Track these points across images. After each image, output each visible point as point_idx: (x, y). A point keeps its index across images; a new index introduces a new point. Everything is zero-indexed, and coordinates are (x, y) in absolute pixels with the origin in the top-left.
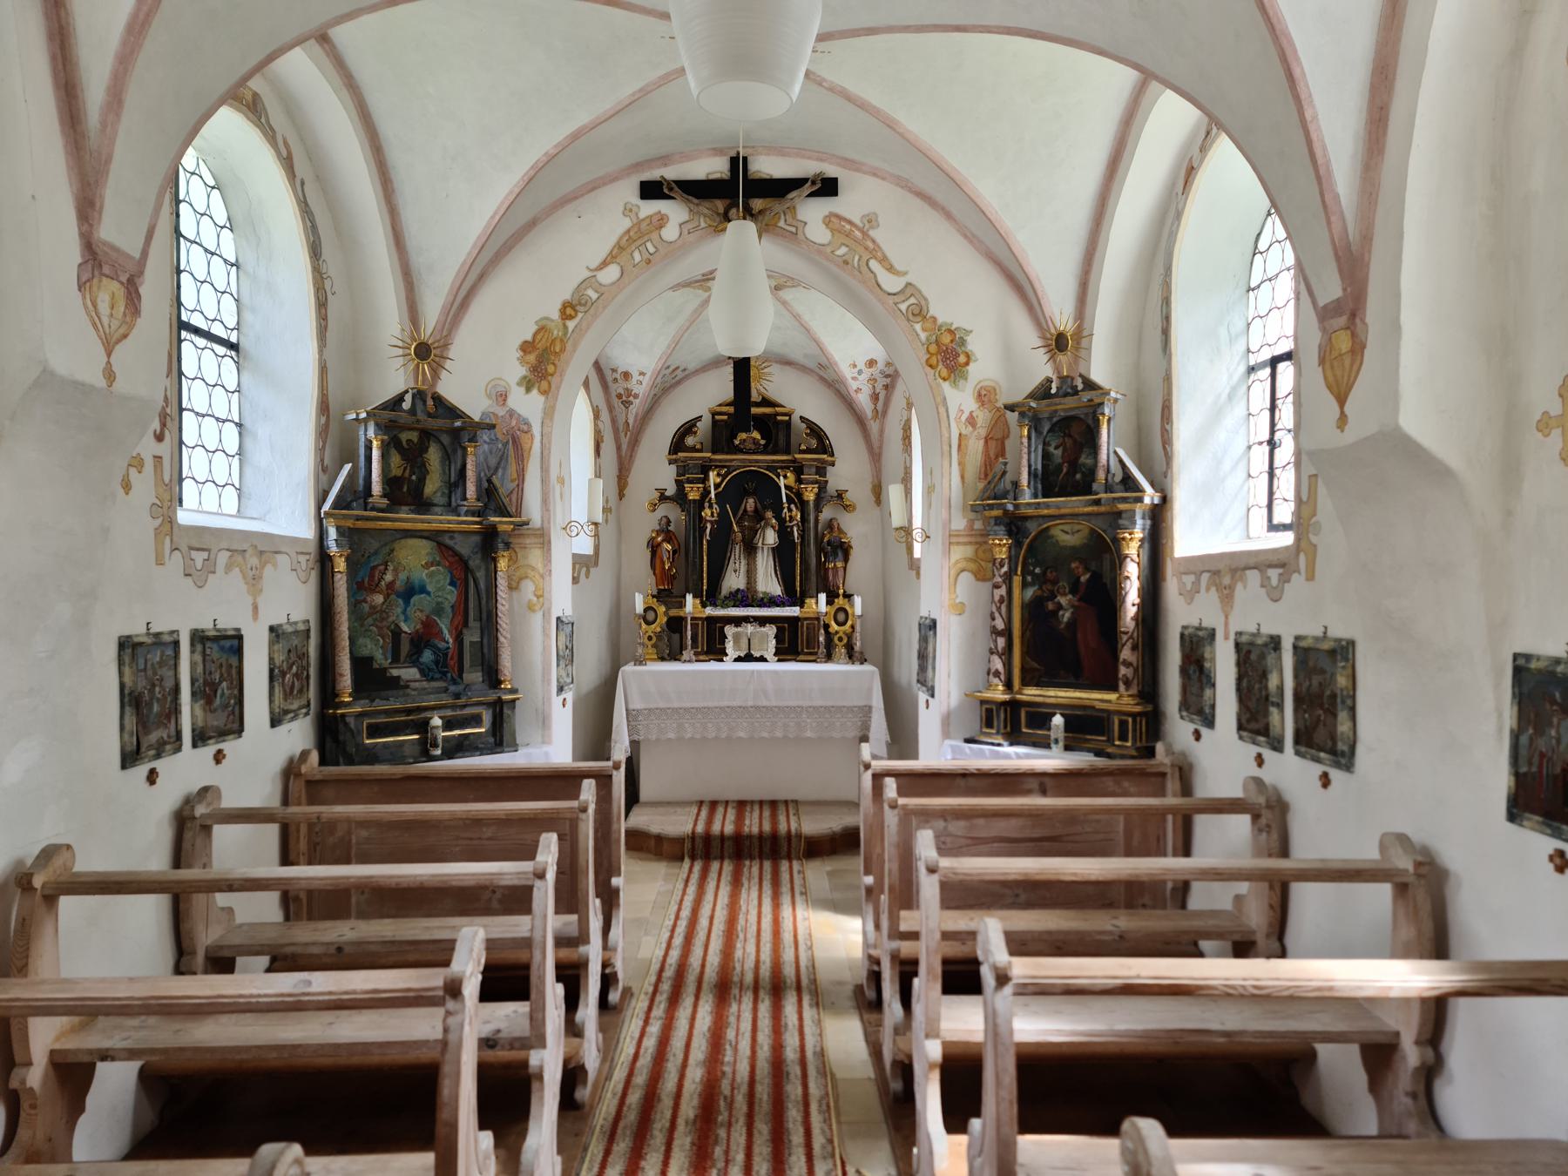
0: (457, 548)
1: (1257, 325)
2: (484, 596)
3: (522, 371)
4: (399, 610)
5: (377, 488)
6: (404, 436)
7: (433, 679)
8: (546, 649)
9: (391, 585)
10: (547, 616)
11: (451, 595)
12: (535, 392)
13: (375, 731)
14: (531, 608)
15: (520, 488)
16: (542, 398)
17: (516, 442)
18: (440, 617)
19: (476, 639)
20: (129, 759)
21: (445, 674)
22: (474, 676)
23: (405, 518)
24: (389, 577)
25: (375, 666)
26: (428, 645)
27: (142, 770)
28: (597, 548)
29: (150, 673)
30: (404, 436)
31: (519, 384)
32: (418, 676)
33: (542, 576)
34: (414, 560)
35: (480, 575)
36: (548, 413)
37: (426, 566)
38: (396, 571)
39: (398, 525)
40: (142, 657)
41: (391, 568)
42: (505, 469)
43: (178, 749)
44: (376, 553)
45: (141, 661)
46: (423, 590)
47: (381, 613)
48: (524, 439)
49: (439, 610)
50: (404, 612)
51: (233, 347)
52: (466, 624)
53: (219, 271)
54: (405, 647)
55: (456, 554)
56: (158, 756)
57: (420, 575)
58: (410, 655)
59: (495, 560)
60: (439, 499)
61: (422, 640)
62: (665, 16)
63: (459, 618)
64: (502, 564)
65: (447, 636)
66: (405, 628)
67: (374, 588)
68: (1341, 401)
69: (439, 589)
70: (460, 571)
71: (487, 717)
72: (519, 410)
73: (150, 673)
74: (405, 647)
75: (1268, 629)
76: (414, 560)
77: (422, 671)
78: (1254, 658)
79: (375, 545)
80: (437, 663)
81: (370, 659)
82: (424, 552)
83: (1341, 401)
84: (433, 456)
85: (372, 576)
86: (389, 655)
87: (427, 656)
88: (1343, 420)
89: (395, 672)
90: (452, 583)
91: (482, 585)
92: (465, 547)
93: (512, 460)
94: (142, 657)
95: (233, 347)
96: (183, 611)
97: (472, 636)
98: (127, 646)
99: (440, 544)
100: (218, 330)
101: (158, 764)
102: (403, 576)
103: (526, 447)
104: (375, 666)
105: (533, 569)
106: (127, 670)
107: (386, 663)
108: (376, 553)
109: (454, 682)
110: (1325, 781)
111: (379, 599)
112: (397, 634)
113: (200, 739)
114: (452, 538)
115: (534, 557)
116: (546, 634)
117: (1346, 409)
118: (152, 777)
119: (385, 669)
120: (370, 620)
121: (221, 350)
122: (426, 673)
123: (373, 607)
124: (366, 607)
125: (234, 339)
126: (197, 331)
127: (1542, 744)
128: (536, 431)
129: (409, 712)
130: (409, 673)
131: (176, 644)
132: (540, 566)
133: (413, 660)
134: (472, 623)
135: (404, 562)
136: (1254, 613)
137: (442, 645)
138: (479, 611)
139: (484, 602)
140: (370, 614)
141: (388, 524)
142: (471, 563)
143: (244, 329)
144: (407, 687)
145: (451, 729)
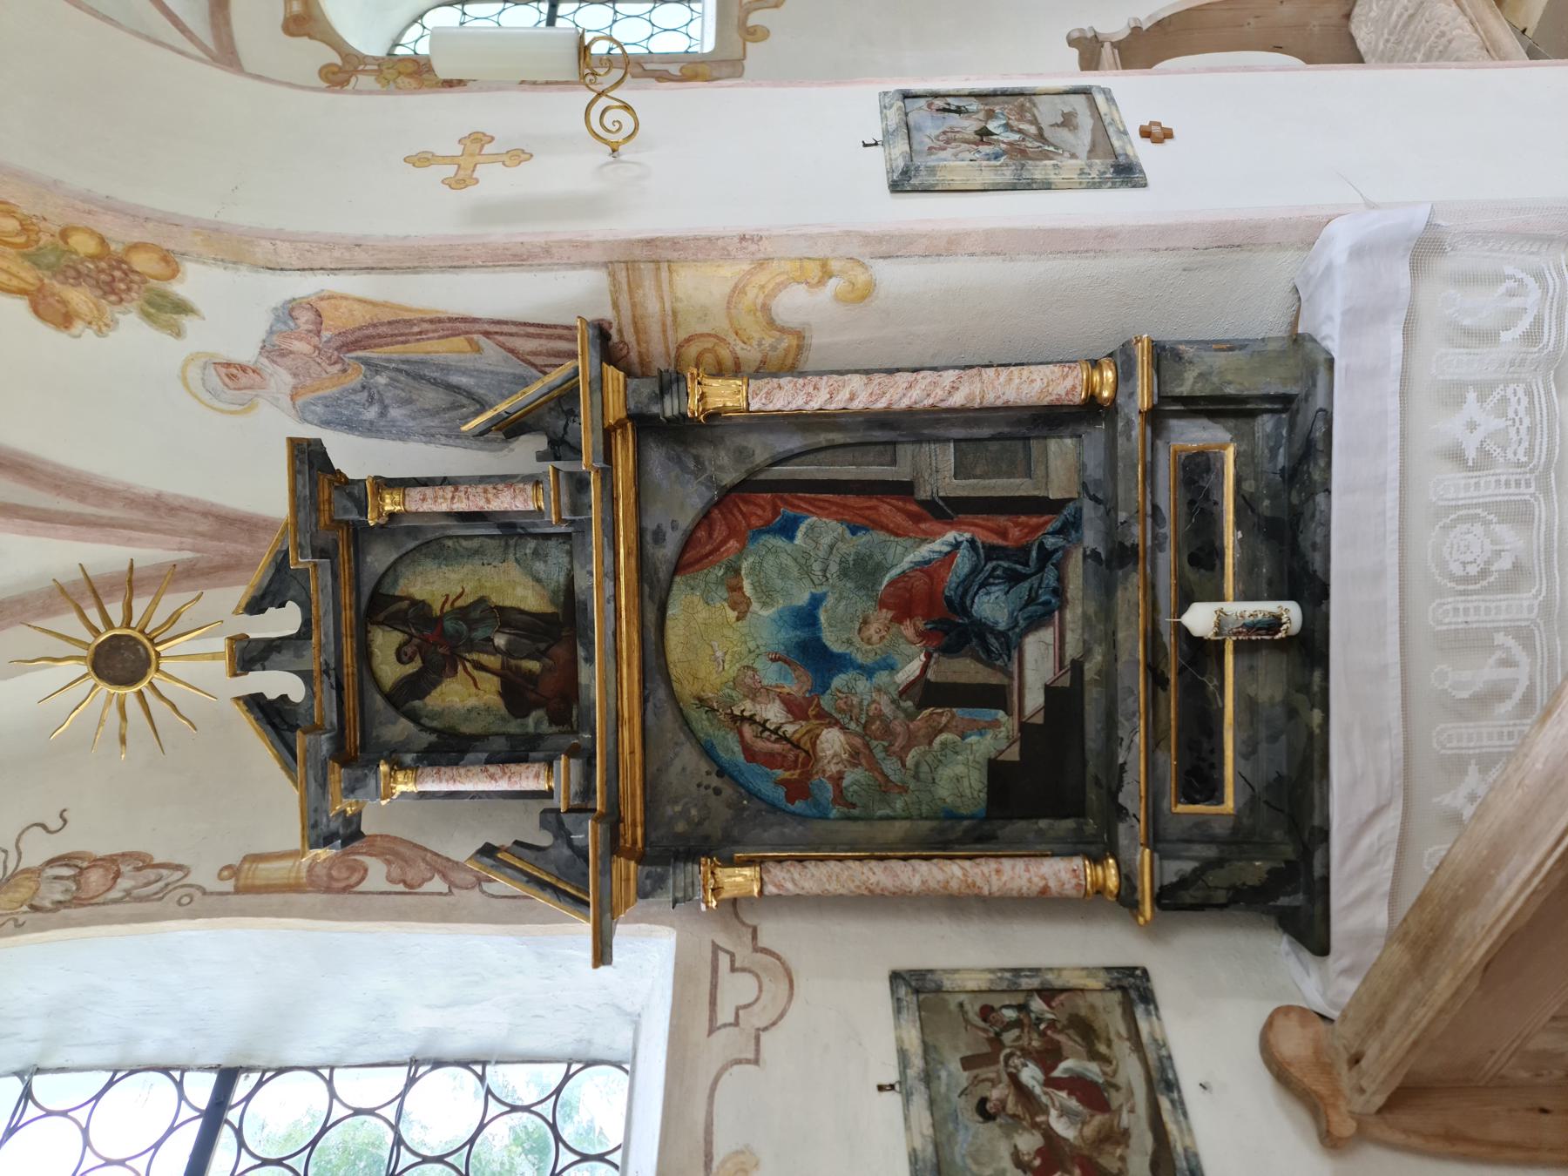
0: (686, 520)
2: (823, 438)
3: (131, 326)
4: (862, 685)
5: (529, 779)
6: (390, 670)
7: (1059, 592)
8: (997, 245)
9: (796, 709)
10: (892, 246)
11: (822, 532)
12: (180, 289)
13: (1200, 780)
14: (862, 295)
15: (495, 329)
16: (190, 269)
17: (353, 342)
18: (881, 569)
19: (947, 457)
21: (1045, 555)
22: (1061, 465)
23: (606, 680)
24: (773, 713)
25: (1013, 754)
26: (960, 605)
30: (390, 670)
31: (178, 333)
32: (1048, 635)
33: (762, 263)
34: (722, 640)
35: (761, 448)
36: (233, 248)
37: (741, 607)
38: (754, 694)
39: (629, 705)
41: (748, 707)
42: (446, 368)
44: (708, 751)
46: (807, 617)
47: (871, 735)
48: (337, 321)
49: (862, 571)
50: (868, 672)
51: (227, 1077)
52: (904, 489)
54: (965, 670)
55: (705, 518)
57: (765, 624)
58: (988, 658)
59: (714, 416)
60: (554, 567)
61: (952, 628)
63: (887, 509)
64: (724, 394)
65: (939, 545)
66: (912, 669)
67: (806, 755)
69: (806, 571)
70: (759, 500)
71: (1192, 435)
72: (260, 332)
74: (965, 670)
76: (722, 640)
77: (1036, 623)
79: (686, 763)
80: (1013, 579)
81: (996, 770)
82: (703, 613)
84: (433, 585)
85: (771, 760)
86: (986, 714)
87: (992, 607)
89: (1034, 700)
90: (787, 530)
91: (794, 443)
92: (681, 501)
93: (415, 351)
97: (939, 470)
99: (680, 567)
102: (770, 674)
103: (361, 316)
104: (1013, 754)
105: (738, 290)
107: (1008, 724)
108: (708, 751)
109: (1072, 526)
111: (832, 741)
112: (927, 693)
114: (659, 536)
115: (701, 290)
116: (946, 246)
119: (1024, 727)
120: (890, 767)
122: (1040, 613)
123: (855, 757)
124: (852, 776)
128: (306, 286)
129: (1157, 679)
130: (1038, 661)
132: (729, 273)
133: (1001, 646)
134: (899, 472)
135: (731, 670)
137: (963, 563)
138: (858, 467)
139: (838, 438)
140: (874, 765)
141: (629, 737)
142: (730, 478)
143: (181, 1057)
144: (1077, 667)
145: (1219, 554)
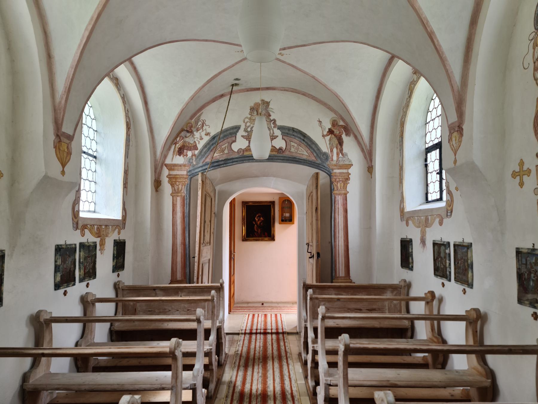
1: (428, 134)
20: (57, 287)
27: (62, 291)
28: (124, 217)
29: (529, 266)
40: (63, 252)
43: (74, 285)
45: (524, 261)
51: (95, 157)
53: (92, 134)
56: (68, 286)
62: (240, 46)
68: (64, 166)
73: (529, 266)
75: (445, 239)
78: (439, 247)
83: (64, 166)
88: (63, 173)
94: (63, 252)
95: (95, 157)
96: (75, 238)
98: (59, 249)
100: (90, 152)
101: (68, 289)
106: (448, 264)
110: (464, 292)
113: (81, 281)
117: (65, 169)
118: (65, 293)
121: (91, 158)
125: (95, 155)
126: (84, 153)
127: (65, 266)
131: (76, 248)
136: (436, 233)
